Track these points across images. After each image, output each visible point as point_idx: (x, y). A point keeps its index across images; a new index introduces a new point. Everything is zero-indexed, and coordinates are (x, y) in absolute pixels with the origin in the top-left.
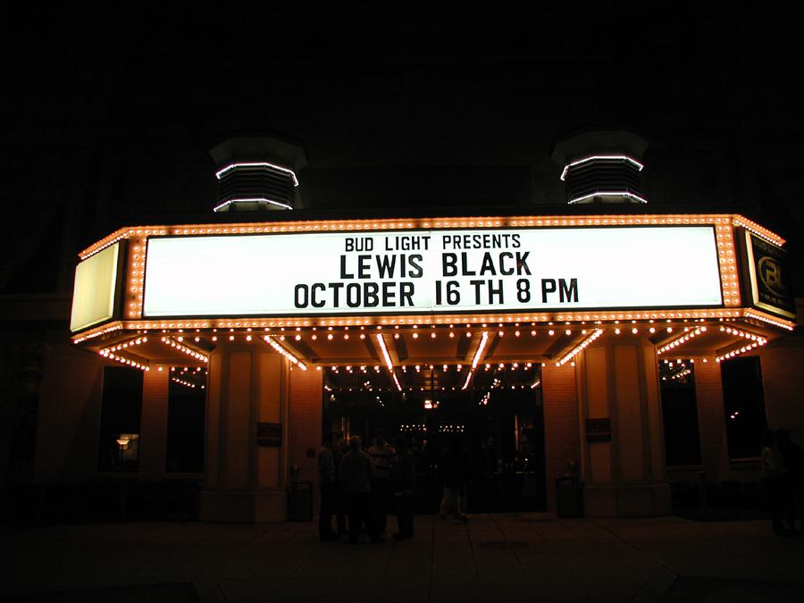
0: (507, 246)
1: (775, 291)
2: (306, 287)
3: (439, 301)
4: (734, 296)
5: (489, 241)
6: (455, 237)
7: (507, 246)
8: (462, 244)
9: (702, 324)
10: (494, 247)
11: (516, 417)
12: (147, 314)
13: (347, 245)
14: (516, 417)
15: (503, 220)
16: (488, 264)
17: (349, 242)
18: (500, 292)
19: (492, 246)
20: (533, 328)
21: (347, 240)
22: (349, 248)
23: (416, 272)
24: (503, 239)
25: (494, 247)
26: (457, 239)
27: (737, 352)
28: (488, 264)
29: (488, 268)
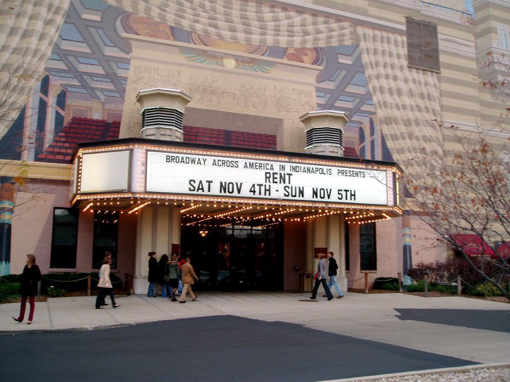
1: (91, 284)
2: (323, 189)
3: (221, 192)
4: (391, 203)
5: (276, 178)
6: (172, 156)
8: (271, 179)
10: (280, 183)
11: (84, 211)
13: (167, 159)
14: (84, 211)
15: (225, 18)
16: (201, 187)
17: (168, 157)
19: (279, 182)
20: (208, 203)
21: (266, 173)
22: (168, 160)
23: (287, 188)
24: (287, 177)
25: (280, 183)
26: (173, 158)
27: (257, 218)
28: (201, 187)
29: (201, 189)
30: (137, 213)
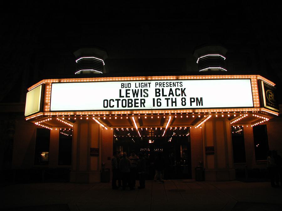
2: (107, 100)
3: (154, 105)
4: (257, 104)
5: (171, 84)
6: (159, 83)
8: (162, 85)
10: (173, 86)
11: (181, 146)
13: (122, 86)
14: (181, 146)
15: (176, 77)
16: (171, 92)
17: (123, 85)
19: (172, 86)
20: (187, 115)
21: (122, 84)
22: (123, 87)
23: (146, 95)
24: (176, 84)
25: (173, 86)
26: (160, 84)
28: (171, 92)
29: (171, 94)
30: (201, 127)
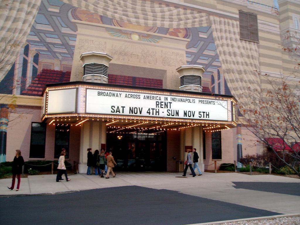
0: (204, 117)
2: (190, 112)
3: (130, 113)
4: (230, 120)
5: (163, 105)
6: (101, 92)
7: (204, 117)
8: (160, 106)
9: (118, 120)
10: (165, 108)
11: (49, 124)
12: (87, 112)
13: (98, 94)
14: (49, 124)
15: (132, 10)
16: (118, 110)
17: (99, 93)
18: (158, 112)
19: (164, 107)
20: (122, 120)
21: (157, 102)
22: (99, 94)
23: (169, 111)
24: (169, 104)
25: (165, 108)
26: (102, 93)
28: (118, 110)
29: (118, 111)
30: (80, 125)
